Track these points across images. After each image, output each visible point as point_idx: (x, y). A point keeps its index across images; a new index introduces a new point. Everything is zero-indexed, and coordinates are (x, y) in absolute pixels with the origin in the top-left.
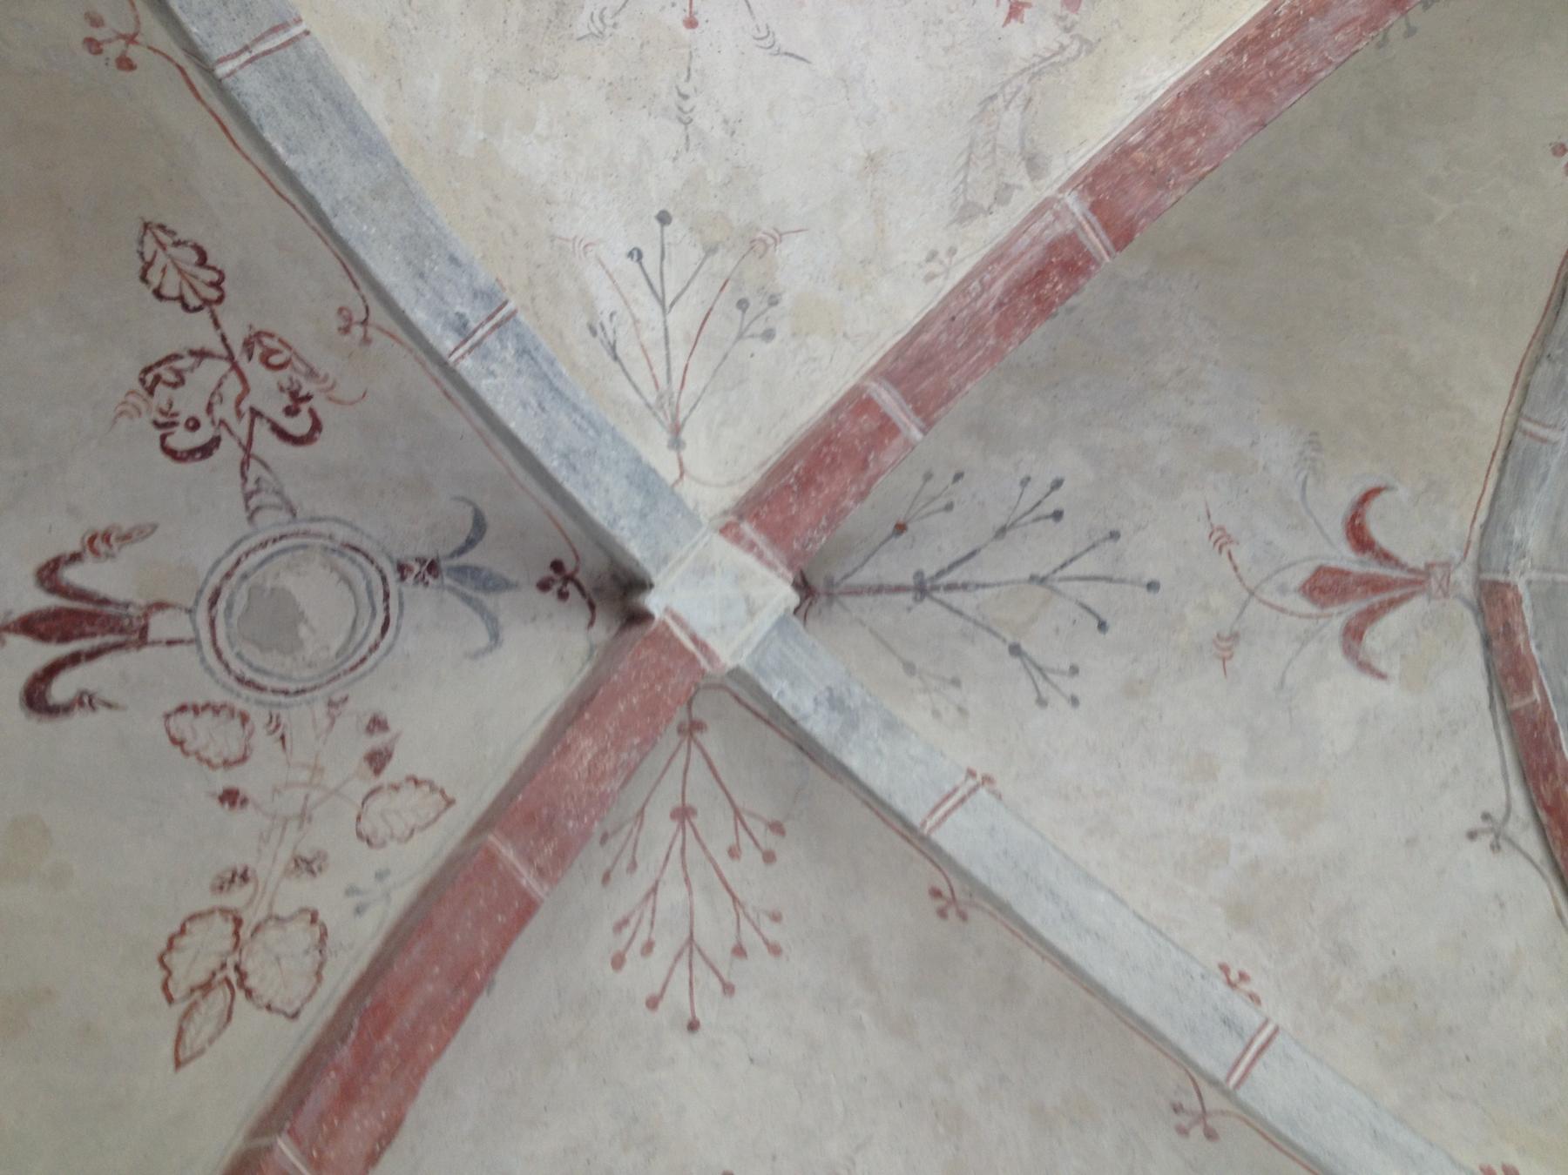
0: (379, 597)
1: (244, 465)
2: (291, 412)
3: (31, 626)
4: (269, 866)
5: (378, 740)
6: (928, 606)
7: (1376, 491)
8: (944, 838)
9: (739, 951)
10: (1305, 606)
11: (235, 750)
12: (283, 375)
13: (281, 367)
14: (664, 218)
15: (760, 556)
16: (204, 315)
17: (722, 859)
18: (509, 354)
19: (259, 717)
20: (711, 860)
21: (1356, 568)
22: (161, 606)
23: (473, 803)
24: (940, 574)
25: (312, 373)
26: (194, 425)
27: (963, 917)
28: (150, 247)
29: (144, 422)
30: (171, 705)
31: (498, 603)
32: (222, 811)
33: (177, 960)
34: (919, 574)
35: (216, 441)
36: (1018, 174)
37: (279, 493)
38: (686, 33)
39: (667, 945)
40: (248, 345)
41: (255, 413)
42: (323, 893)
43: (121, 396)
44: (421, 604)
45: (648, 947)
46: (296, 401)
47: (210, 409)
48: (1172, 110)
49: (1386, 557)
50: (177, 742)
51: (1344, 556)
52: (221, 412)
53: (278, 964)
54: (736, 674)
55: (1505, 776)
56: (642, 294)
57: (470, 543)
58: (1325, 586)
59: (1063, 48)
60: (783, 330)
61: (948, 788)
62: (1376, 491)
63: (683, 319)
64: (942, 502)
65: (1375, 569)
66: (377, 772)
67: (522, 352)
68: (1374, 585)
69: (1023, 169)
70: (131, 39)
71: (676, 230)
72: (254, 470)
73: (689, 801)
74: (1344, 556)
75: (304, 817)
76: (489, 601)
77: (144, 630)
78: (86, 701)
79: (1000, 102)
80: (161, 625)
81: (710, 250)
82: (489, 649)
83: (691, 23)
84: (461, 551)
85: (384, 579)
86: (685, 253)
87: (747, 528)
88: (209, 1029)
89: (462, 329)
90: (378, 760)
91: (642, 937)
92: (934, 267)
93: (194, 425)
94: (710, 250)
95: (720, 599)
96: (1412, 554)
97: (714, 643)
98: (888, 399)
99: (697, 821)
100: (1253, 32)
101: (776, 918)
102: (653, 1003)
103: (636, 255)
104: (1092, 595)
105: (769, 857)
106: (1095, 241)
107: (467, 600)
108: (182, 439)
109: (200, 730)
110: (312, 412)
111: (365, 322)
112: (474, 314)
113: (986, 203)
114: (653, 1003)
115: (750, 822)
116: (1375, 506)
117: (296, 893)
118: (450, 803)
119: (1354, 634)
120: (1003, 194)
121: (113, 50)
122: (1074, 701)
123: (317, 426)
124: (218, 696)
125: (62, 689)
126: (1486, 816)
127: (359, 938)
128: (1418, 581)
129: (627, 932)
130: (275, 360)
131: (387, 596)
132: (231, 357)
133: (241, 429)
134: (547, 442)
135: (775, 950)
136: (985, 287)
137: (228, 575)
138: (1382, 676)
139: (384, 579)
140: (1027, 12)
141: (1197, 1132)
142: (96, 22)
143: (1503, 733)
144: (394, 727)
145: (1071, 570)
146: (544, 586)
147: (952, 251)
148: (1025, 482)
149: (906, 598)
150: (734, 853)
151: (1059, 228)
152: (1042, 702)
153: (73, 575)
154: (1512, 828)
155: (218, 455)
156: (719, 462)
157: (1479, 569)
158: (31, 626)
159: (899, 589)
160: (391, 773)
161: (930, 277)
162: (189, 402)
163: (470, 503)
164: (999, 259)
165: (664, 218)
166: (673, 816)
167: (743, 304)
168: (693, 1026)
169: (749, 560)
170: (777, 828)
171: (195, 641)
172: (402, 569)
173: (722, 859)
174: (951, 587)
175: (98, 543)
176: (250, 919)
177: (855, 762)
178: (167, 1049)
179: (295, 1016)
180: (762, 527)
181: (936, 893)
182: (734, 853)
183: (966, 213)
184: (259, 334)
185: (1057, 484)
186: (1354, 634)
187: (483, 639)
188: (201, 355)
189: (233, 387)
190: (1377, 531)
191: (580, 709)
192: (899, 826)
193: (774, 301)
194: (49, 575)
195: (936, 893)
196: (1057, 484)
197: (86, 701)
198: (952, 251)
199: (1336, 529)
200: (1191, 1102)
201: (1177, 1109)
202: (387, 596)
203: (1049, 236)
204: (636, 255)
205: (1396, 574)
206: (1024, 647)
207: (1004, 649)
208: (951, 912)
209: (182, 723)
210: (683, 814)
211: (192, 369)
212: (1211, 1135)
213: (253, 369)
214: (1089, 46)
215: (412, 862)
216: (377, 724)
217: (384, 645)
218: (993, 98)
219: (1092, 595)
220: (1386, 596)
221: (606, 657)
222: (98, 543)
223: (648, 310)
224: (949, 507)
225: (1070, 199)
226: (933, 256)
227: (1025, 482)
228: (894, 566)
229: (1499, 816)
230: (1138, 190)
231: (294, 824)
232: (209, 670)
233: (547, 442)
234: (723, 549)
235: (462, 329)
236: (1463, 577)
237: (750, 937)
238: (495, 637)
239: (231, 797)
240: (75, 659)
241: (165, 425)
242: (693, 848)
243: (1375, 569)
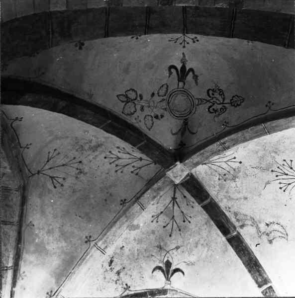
0: (182, 115)
1: (206, 100)
2: (213, 109)
3: (183, 67)
4: (143, 103)
5: (160, 117)
6: (171, 199)
7: (183, 273)
8: (136, 205)
9: (117, 166)
10: (165, 260)
11: (160, 94)
12: (219, 110)
13: (221, 110)
14: (240, 163)
15: (184, 179)
16: (230, 102)
17: (133, 164)
18: (219, 148)
19: (165, 98)
20: (133, 163)
21: (171, 270)
22: (184, 84)
23: (150, 134)
24: (176, 202)
25: (219, 115)
26: (213, 94)
27: (121, 204)
28: (241, 98)
29: (214, 88)
30: (168, 84)
31: (179, 135)
32: (151, 93)
33: (131, 92)
34: (176, 198)
35: (210, 97)
36: (241, 224)
37: (200, 104)
38: (270, 170)
39: (119, 155)
40: (224, 107)
41: (214, 104)
42: (139, 112)
43: (219, 85)
44: (180, 122)
45: (119, 152)
46: (215, 111)
47: (215, 97)
48: (248, 251)
49: (172, 274)
50: (162, 86)
51: (173, 267)
52: (214, 100)
53: (130, 108)
54: (165, 175)
55: (136, 291)
56: (228, 158)
57: (190, 131)
58: (168, 264)
59: (260, 232)
60: (220, 182)
61: (144, 205)
62: (183, 273)
63: (224, 166)
64: (188, 203)
65: (171, 272)
66: (155, 117)
67: (219, 151)
68: (168, 272)
69: (241, 224)
70: (270, 108)
71: (238, 164)
72: (205, 101)
73: (143, 161)
74: (173, 267)
75: (149, 107)
76: (180, 133)
77: (181, 81)
78: (171, 73)
79: (253, 221)
80: (181, 84)
81: (234, 170)
82: (172, 133)
83: (272, 171)
84: (188, 129)
85: (185, 117)
86: (235, 165)
87: (189, 177)
88: (122, 99)
89: (224, 143)
90: (157, 117)
91: (121, 151)
92: (228, 208)
93: (213, 94)
94: (234, 170)
95: (178, 172)
96: (172, 279)
97: (171, 171)
98: (209, 200)
99: (139, 161)
100: (258, 264)
101: (122, 172)
102: (110, 152)
103: (235, 158)
104: (169, 226)
105: (132, 172)
106: (229, 236)
107: (180, 130)
108: (211, 92)
109: (164, 89)
110: (213, 113)
111: (226, 126)
112: (227, 145)
113: (237, 218)
114: (110, 152)
115: (138, 170)
116: (180, 273)
117: (138, 107)
118: (149, 130)
119: (159, 268)
120: (238, 220)
121: (268, 105)
122: (152, 222)
123: (211, 113)
124: (169, 91)
125: (173, 70)
126: (129, 287)
127: (132, 120)
128: (168, 279)
129: (123, 149)
130: (222, 110)
131: (182, 117)
132: (223, 103)
133: (212, 101)
134: (205, 151)
135: (116, 171)
136: (223, 218)
137: (188, 94)
138: (153, 272)
139: (185, 117)
140: (267, 227)
141: (86, 240)
142: (273, 104)
143: (143, 291)
144: (162, 119)
145: (174, 222)
146: (181, 142)
147: (230, 212)
148: (190, 217)
149: (173, 196)
150: (133, 167)
151: (231, 231)
152: (153, 217)
153: (191, 73)
154: (127, 291)
155: (208, 97)
156: (201, 171)
157: (170, 289)
158: (183, 67)
159: (174, 195)
160: (154, 120)
161: (226, 208)
162: (217, 95)
163: (196, 132)
164: (227, 220)
165: (240, 163)
166: (141, 158)
167: (225, 175)
168: (105, 158)
169: (183, 177)
170: (137, 174)
171: (178, 88)
172: (186, 120)
173: (133, 164)
174: (174, 203)
175: (196, 77)
176: (136, 102)
177: (149, 191)
178: (119, 94)
179: (123, 113)
180: (188, 180)
181: (125, 200)
182: (133, 167)
183: (236, 214)
184: (226, 109)
185: (190, 222)
186: (159, 268)
187: (173, 132)
188: (224, 99)
189: (218, 102)
190: (176, 274)
191: (159, 147)
192: (138, 195)
193: (225, 180)
194: (191, 70)
195: (125, 200)
196: (190, 222)
197: (171, 73)
198: (230, 212)
199: (177, 267)
200: (92, 239)
201: (90, 237)
202: (182, 117)
203: (230, 229)
204: (235, 158)
205: (170, 276)
206: (162, 214)
207: (162, 211)
208: (122, 202)
209: (166, 86)
210: (141, 159)
211: (222, 97)
212: (86, 242)
213: (220, 106)
214: (260, 237)
215: (142, 126)
216: (162, 116)
217: (174, 117)
218: (254, 220)
219: (169, 226)
220: (165, 272)
221: (169, 151)
222: (196, 77)
223: (225, 160)
224: (187, 205)
225: (235, 233)
226: (229, 208)
227: (190, 217)
228: (178, 195)
229: (130, 289)
230: (236, 244)
231: (148, 105)
232: (173, 90)
233: (205, 151)
234: (186, 173)
235: (224, 143)
236: (168, 287)
237: (119, 168)
238: (173, 134)
239: (153, 94)
240: (178, 74)
241: (213, 90)
242: (135, 160)
243: (171, 272)
